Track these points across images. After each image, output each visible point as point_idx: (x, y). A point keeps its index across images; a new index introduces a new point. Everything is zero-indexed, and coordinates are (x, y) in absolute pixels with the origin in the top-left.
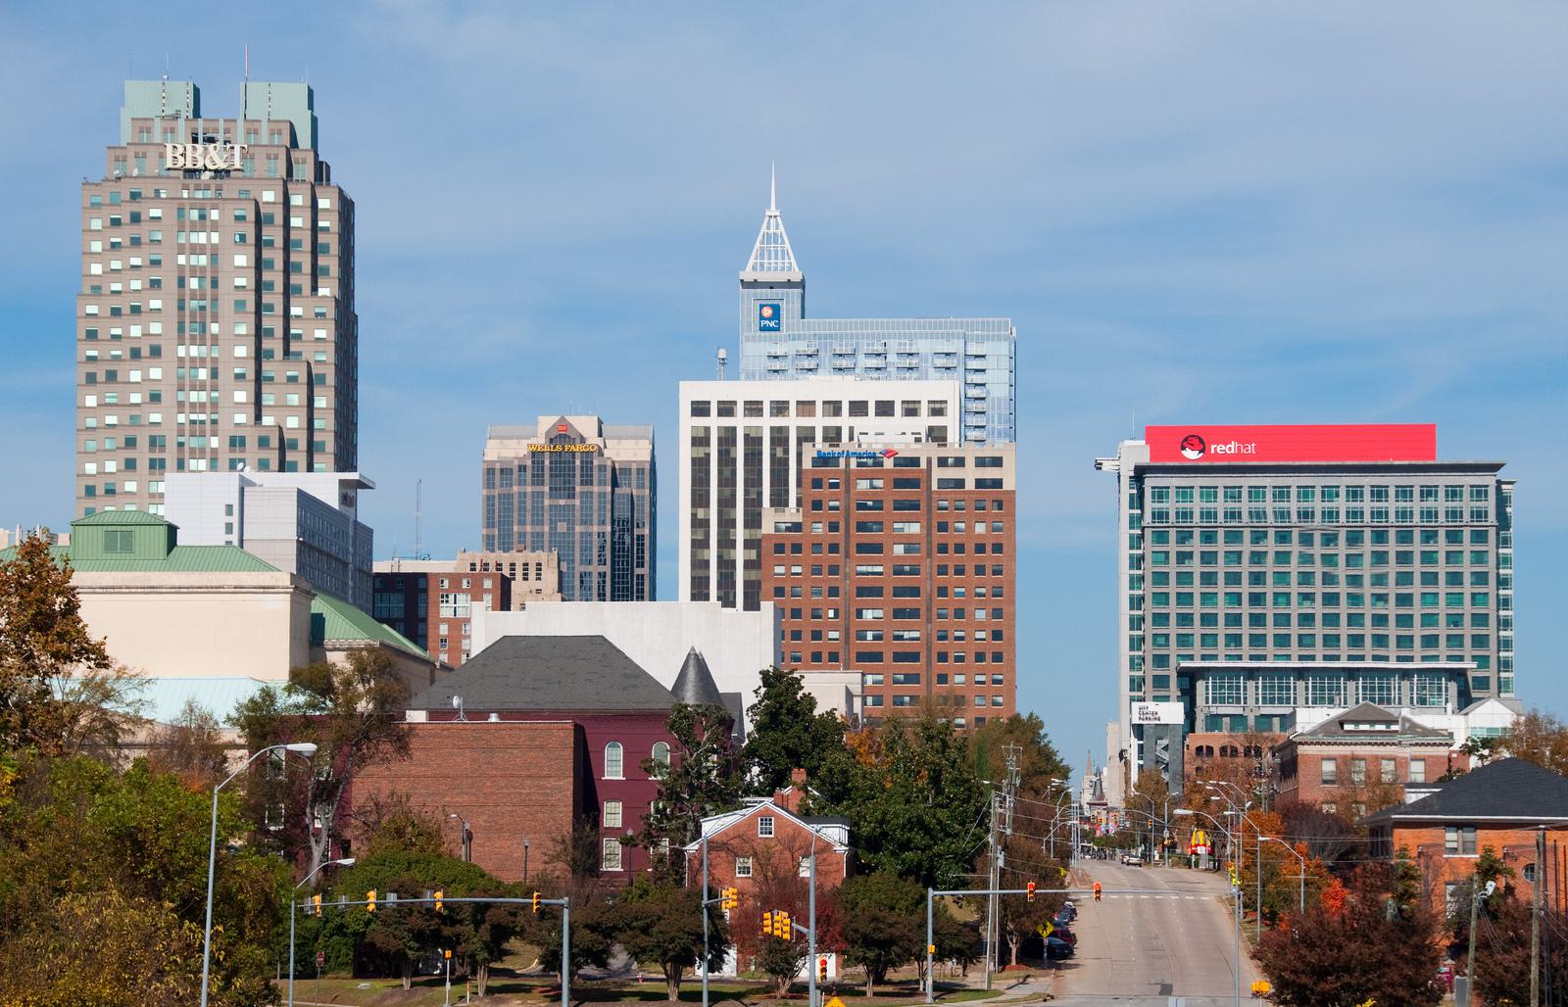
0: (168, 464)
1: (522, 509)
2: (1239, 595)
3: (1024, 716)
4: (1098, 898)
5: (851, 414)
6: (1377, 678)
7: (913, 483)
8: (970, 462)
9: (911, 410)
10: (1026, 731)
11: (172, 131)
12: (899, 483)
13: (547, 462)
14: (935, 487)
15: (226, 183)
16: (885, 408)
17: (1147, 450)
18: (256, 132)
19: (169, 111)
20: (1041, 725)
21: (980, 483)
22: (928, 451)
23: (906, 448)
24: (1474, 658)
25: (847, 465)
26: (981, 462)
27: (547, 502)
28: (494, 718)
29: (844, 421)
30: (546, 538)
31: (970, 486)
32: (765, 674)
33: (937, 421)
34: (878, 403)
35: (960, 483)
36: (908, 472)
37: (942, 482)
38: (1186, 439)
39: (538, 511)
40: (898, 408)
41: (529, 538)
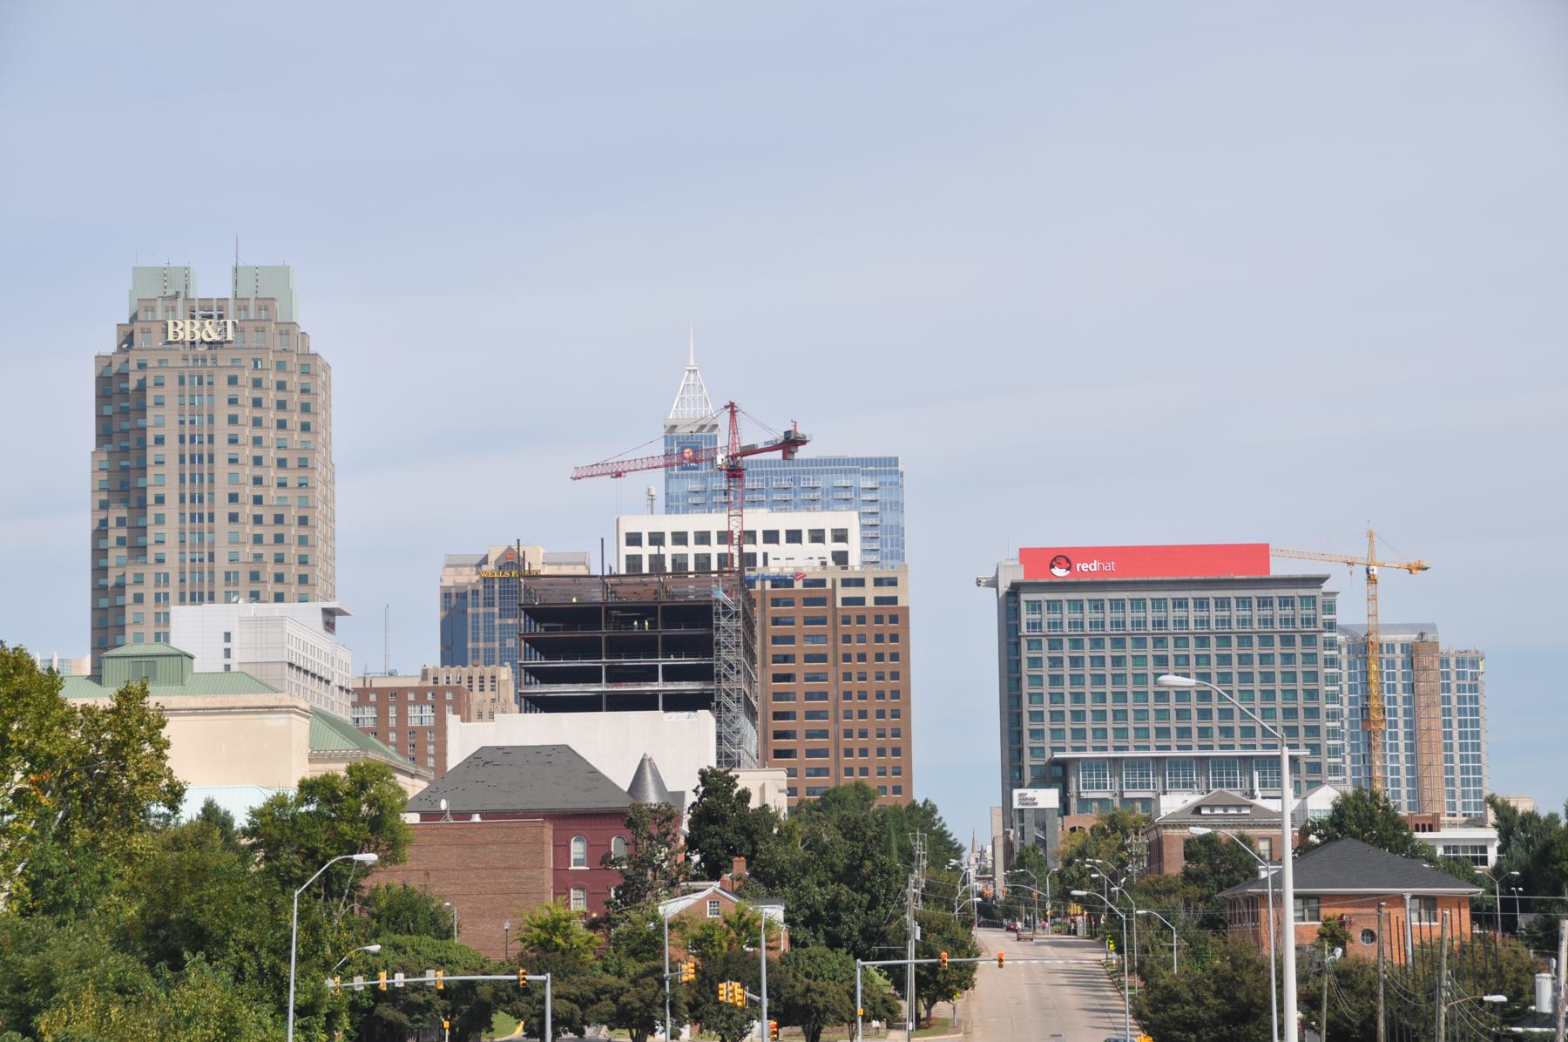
0: (171, 596)
1: (476, 628)
2: (1104, 694)
3: (920, 802)
4: (1001, 966)
5: (766, 541)
6: (1224, 767)
7: (821, 601)
8: (869, 582)
9: (817, 536)
10: (924, 816)
11: (174, 309)
12: (809, 602)
13: (497, 587)
14: (839, 604)
15: (219, 352)
16: (794, 536)
18: (246, 309)
19: (170, 292)
21: (878, 600)
22: (833, 573)
23: (812, 570)
24: (1307, 746)
25: (763, 586)
26: (878, 582)
27: (497, 621)
28: (477, 818)
29: (759, 548)
30: (497, 653)
31: (870, 603)
32: (702, 773)
33: (840, 547)
34: (788, 532)
35: (861, 601)
36: (816, 591)
37: (846, 601)
39: (490, 628)
40: (805, 536)
41: (482, 653)
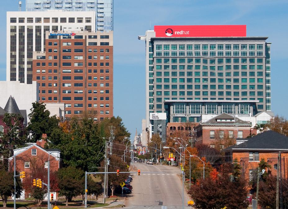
2: (184, 79)
4: (139, 175)
5: (61, 22)
17: (155, 33)
20: (121, 120)
24: (258, 99)
34: (69, 18)
38: (167, 30)
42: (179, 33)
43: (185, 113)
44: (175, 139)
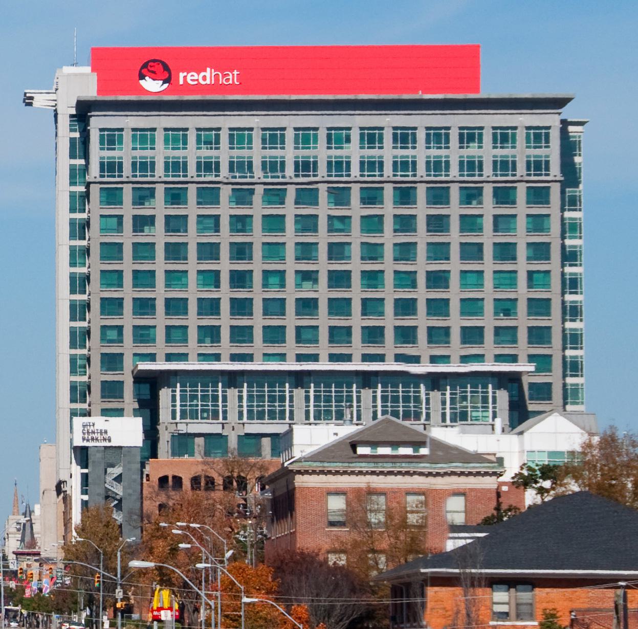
24: (531, 358)
38: (145, 66)
42: (196, 77)
43: (221, 420)
44: (181, 528)
